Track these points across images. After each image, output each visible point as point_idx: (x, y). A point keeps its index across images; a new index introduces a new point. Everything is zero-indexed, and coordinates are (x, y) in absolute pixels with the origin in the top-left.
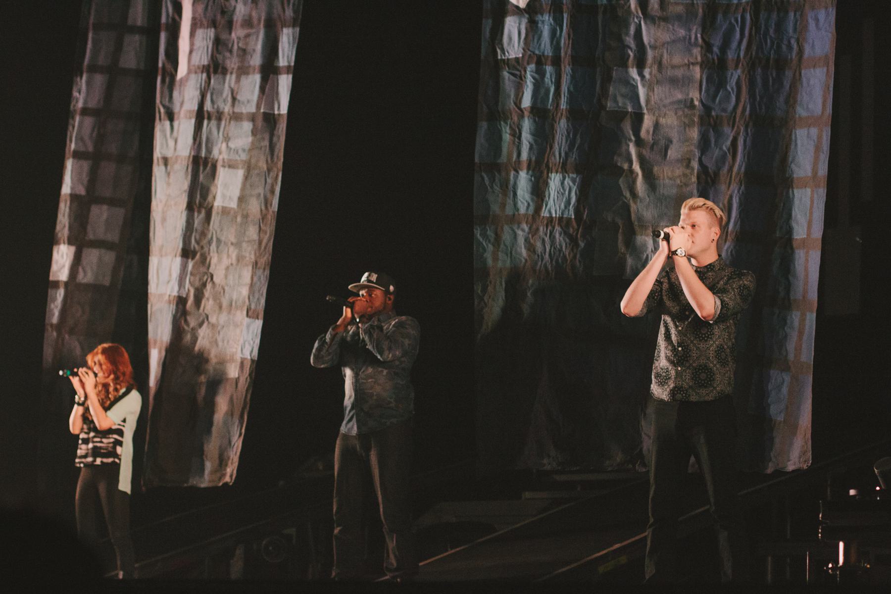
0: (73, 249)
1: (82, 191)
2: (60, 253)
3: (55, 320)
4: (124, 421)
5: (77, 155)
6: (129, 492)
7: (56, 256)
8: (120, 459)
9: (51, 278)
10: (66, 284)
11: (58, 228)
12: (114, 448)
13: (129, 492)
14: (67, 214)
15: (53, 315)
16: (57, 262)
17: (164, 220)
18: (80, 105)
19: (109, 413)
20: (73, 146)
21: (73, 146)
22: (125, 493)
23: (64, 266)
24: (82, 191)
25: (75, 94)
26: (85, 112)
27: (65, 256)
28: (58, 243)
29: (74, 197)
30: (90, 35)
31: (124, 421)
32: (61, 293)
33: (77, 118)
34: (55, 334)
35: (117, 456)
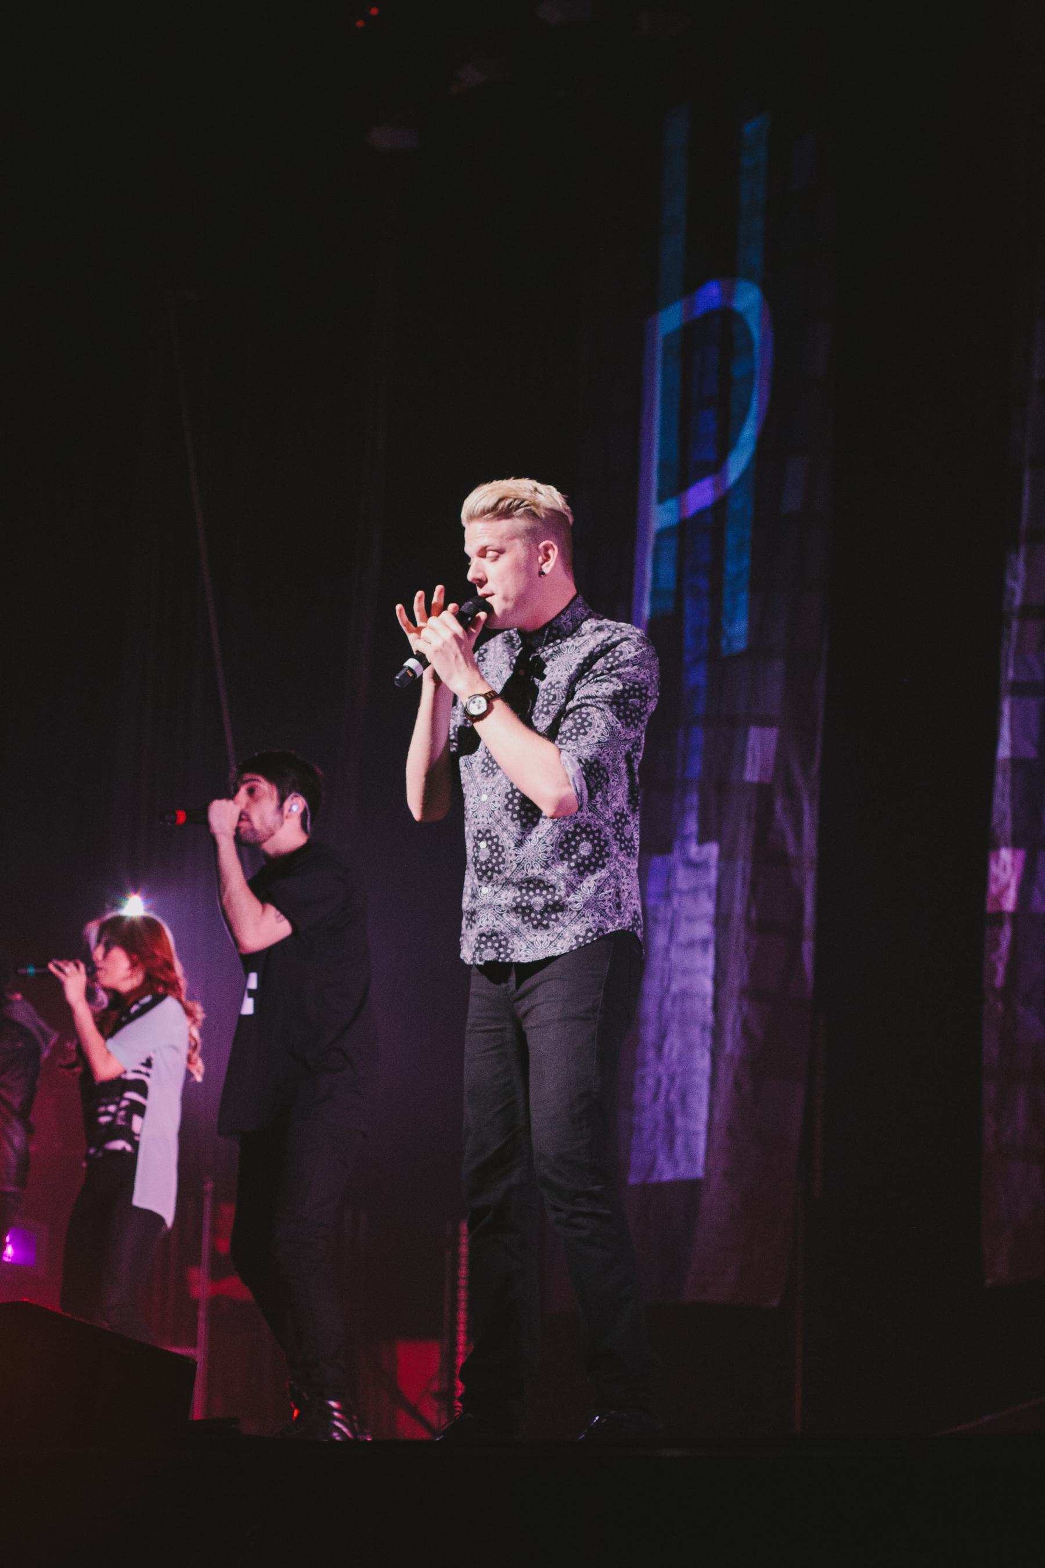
0: (1021, 854)
1: (1030, 751)
2: (1001, 863)
3: (999, 980)
4: (148, 1064)
5: (1018, 689)
6: (168, 1214)
7: (994, 869)
8: (136, 1145)
9: (990, 908)
10: (1015, 916)
11: (996, 819)
12: (129, 1120)
13: (168, 1214)
14: (1007, 795)
15: (995, 972)
16: (997, 879)
17: (456, 657)
18: (1018, 601)
19: (110, 1043)
20: (1011, 673)
21: (1011, 673)
22: (153, 1219)
23: (1007, 886)
24: (1030, 751)
25: (1010, 583)
26: (1027, 611)
27: (1009, 868)
28: (997, 848)
29: (1015, 762)
30: (1027, 477)
31: (148, 1064)
32: (1006, 934)
33: (1015, 624)
34: (1000, 1006)
35: (132, 1138)
